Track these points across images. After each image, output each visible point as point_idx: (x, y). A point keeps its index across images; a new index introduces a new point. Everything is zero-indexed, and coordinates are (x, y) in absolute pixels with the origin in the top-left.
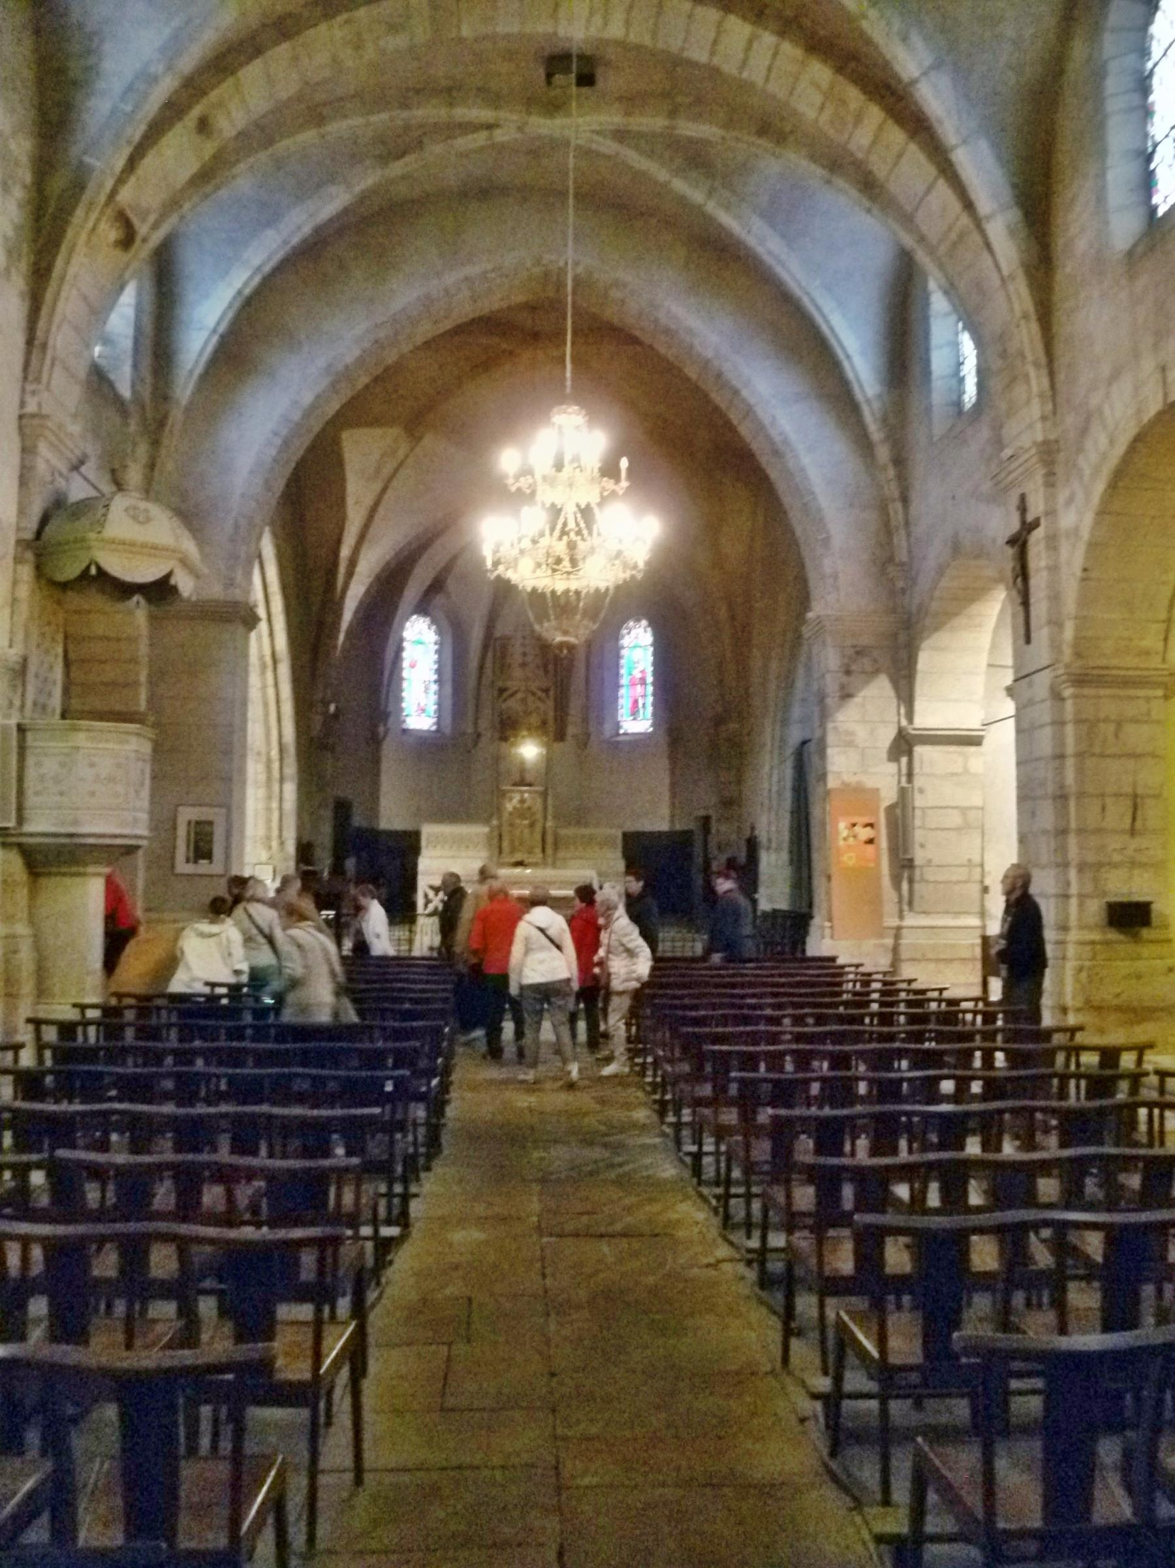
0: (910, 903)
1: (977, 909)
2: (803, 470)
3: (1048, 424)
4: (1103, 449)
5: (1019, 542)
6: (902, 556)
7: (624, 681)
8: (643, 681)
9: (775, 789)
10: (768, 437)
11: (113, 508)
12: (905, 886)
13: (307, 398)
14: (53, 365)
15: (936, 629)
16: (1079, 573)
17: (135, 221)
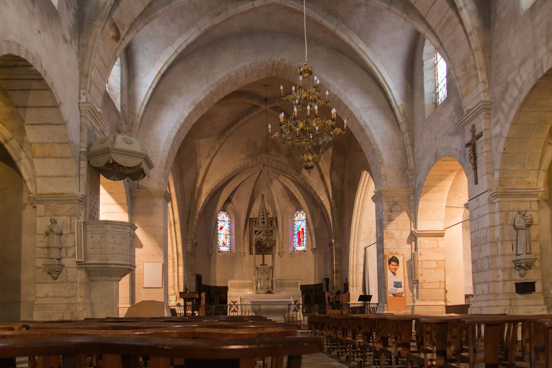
0: (417, 297)
1: (443, 299)
2: (372, 135)
3: (486, 93)
4: (516, 95)
5: (472, 145)
6: (411, 166)
10: (359, 124)
12: (415, 290)
13: (186, 114)
14: (91, 84)
15: (426, 193)
16: (502, 151)
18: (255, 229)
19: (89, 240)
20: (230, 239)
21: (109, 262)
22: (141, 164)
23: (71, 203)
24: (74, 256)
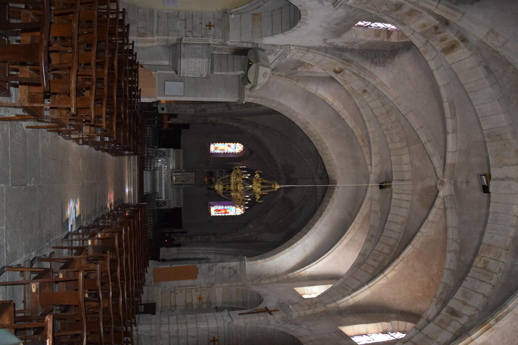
6: (263, 282)
7: (226, 207)
8: (226, 213)
11: (267, 68)
17: (340, 74)
18: (224, 171)
19: (197, 47)
21: (182, 59)
23: (222, 35)
24: (186, 36)
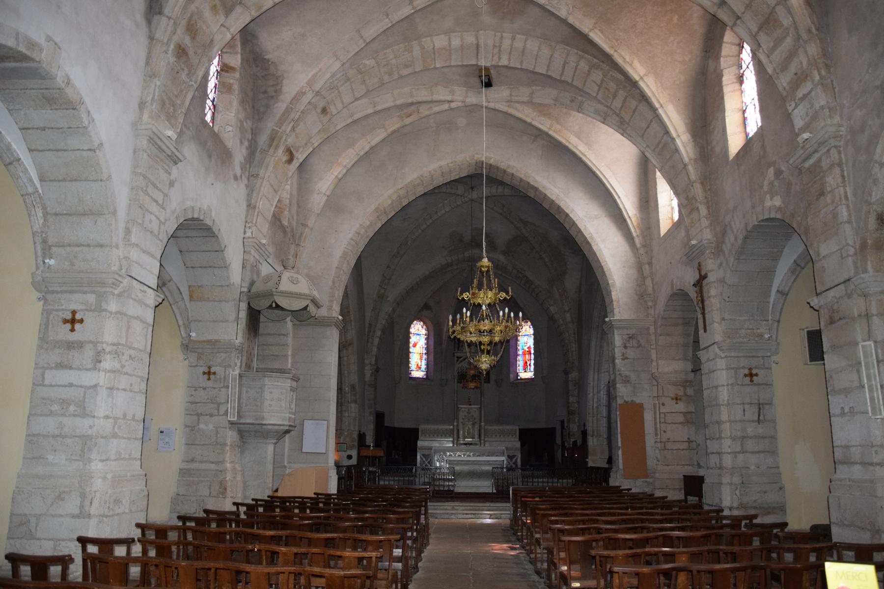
2: (600, 250)
7: (520, 352)
9: (595, 405)
19: (244, 396)
20: (428, 360)
21: (264, 422)
22: (307, 306)
24: (226, 414)
